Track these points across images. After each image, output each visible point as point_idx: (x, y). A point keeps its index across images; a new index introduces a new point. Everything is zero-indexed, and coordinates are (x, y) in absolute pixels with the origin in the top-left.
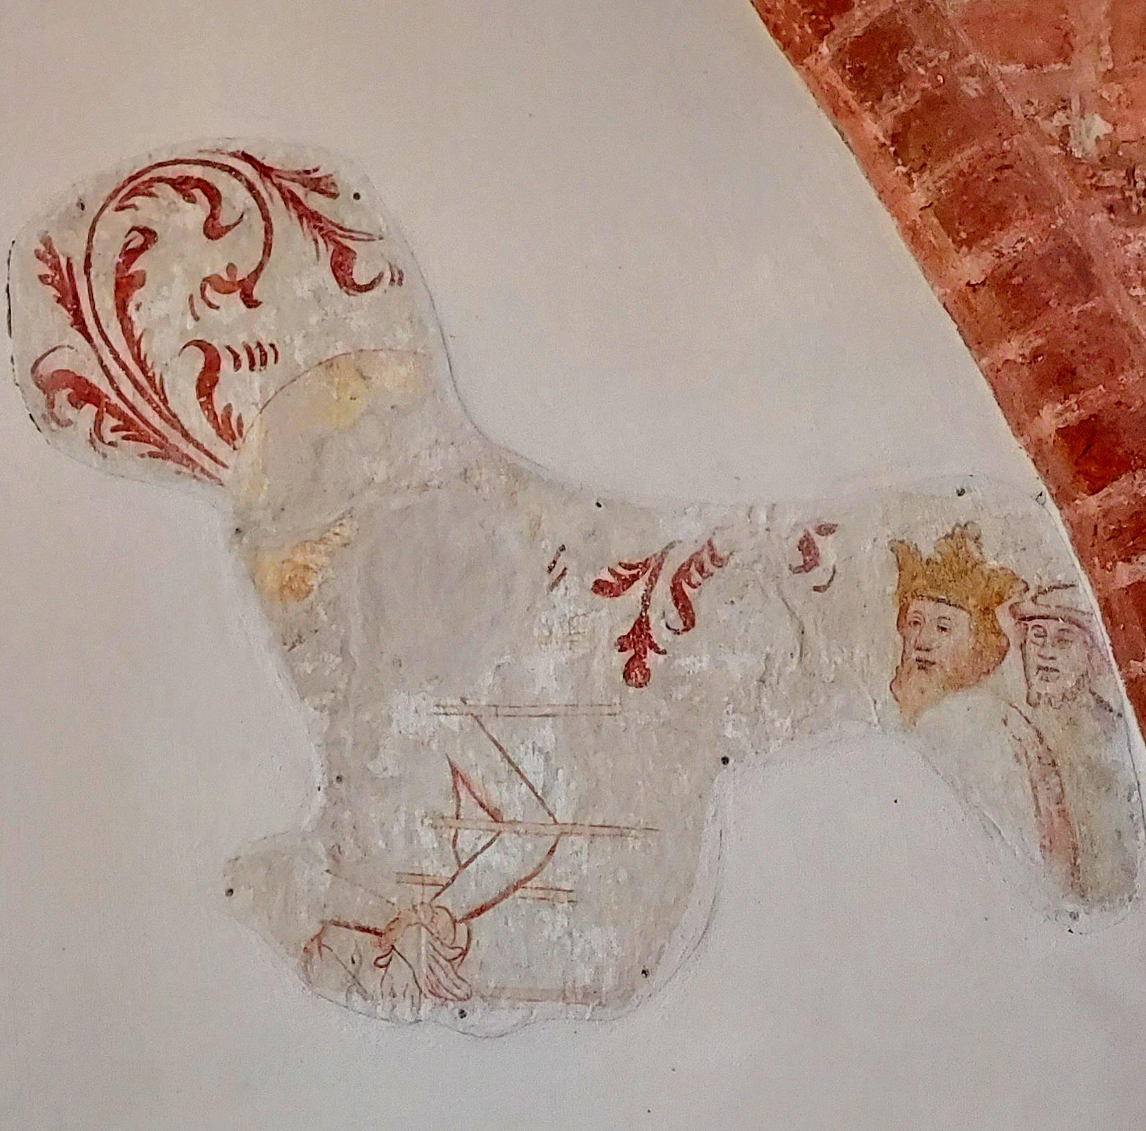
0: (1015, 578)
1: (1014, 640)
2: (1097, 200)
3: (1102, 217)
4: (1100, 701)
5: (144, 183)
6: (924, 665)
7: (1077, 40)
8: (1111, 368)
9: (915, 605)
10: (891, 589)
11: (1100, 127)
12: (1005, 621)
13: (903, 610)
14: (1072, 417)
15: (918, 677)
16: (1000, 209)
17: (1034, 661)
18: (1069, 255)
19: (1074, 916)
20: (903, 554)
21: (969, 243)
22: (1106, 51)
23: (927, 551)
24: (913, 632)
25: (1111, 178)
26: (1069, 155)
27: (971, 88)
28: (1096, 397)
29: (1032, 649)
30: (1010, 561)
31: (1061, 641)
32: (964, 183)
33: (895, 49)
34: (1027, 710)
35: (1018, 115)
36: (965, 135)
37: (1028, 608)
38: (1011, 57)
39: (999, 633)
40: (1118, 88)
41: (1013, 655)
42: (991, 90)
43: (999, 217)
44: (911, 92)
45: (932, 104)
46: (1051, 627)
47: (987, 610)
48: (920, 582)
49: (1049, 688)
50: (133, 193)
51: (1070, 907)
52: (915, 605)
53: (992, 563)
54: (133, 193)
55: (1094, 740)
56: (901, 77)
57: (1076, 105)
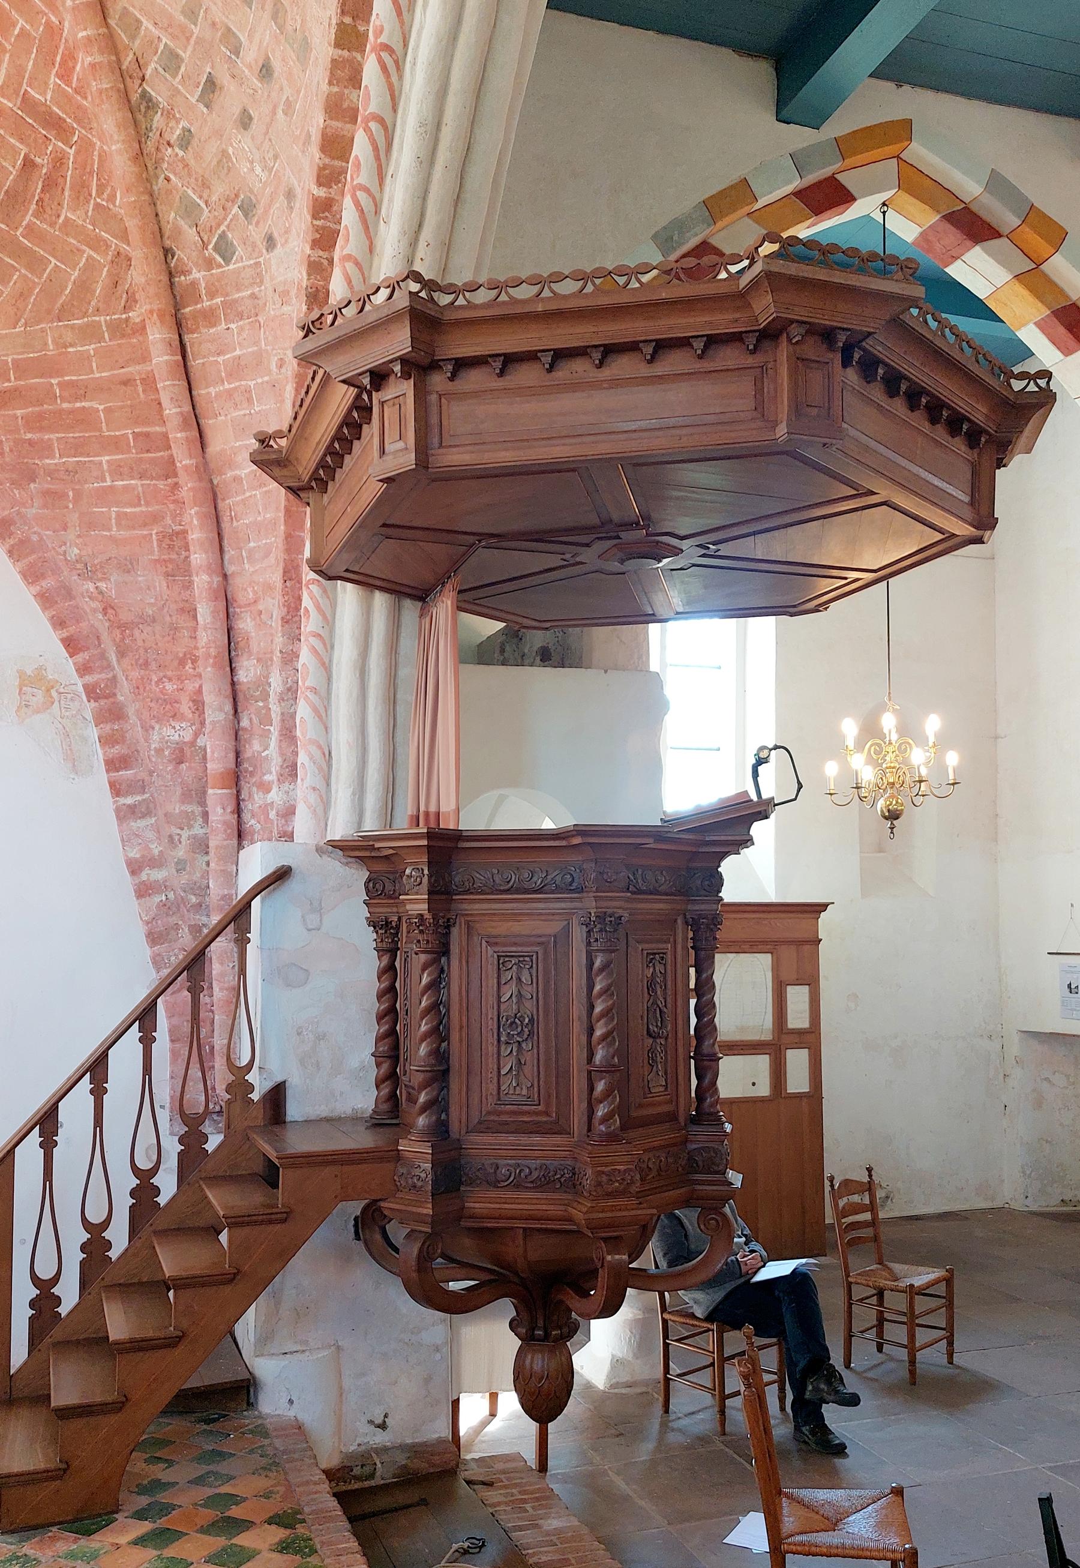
0: (57, 682)
1: (56, 699)
2: (75, 572)
3: (76, 577)
4: (84, 718)
5: (575, 1541)
6: (27, 706)
7: (69, 525)
8: (78, 622)
9: (24, 688)
10: (17, 684)
11: (76, 551)
12: (54, 693)
13: (21, 690)
14: (64, 635)
15: (24, 709)
16: (42, 574)
17: (63, 705)
18: (64, 588)
19: (74, 779)
20: (21, 674)
21: (32, 583)
22: (78, 528)
23: (29, 672)
24: (24, 697)
25: (79, 566)
26: (66, 559)
27: (35, 538)
28: (72, 629)
29: (62, 702)
30: (56, 676)
31: (72, 700)
32: (31, 566)
33: (10, 525)
34: (60, 720)
35: (50, 545)
36: (33, 552)
37: (62, 690)
38: (48, 529)
39: (51, 697)
40: (81, 540)
41: (56, 704)
42: (42, 539)
43: (43, 576)
44: (15, 538)
45: (21, 542)
46: (69, 696)
47: (48, 690)
48: (26, 682)
49: (68, 713)
50: (250, 1066)
51: (72, 777)
52: (24, 688)
53: (51, 677)
54: (250, 1066)
55: (81, 729)
56: (11, 534)
57: (68, 544)
